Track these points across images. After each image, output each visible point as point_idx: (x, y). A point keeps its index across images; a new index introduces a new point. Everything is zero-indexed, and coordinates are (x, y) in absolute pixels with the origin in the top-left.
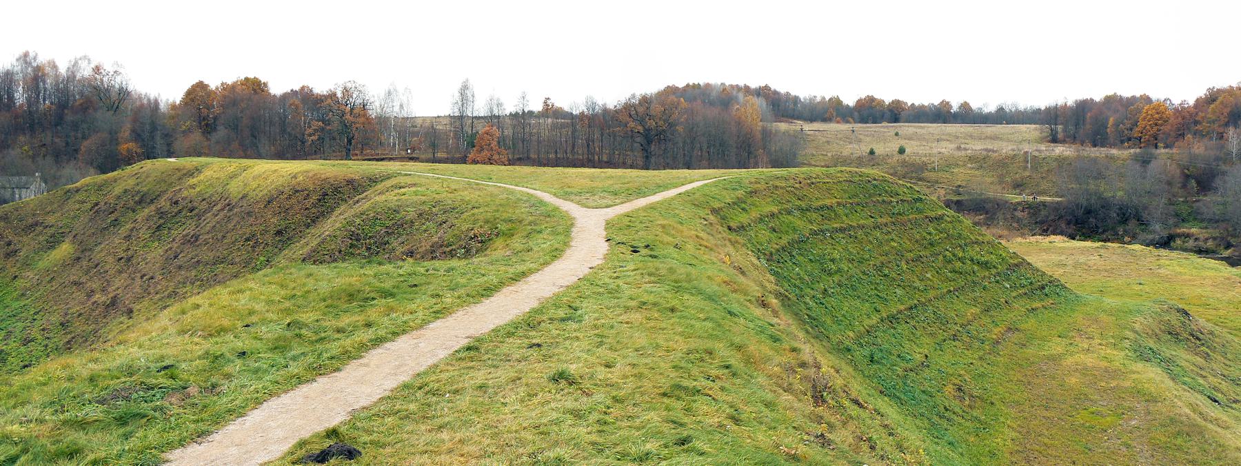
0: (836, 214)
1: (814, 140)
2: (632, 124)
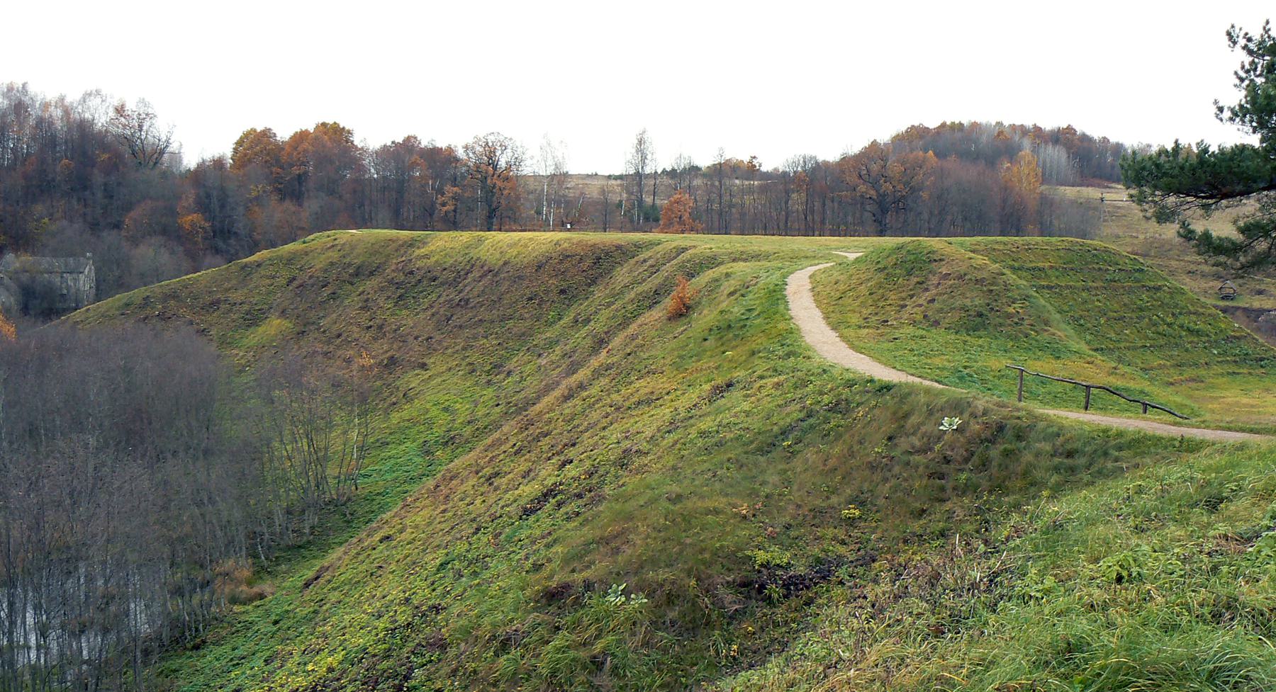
0: (1046, 275)
1: (1125, 216)
2: (862, 188)
